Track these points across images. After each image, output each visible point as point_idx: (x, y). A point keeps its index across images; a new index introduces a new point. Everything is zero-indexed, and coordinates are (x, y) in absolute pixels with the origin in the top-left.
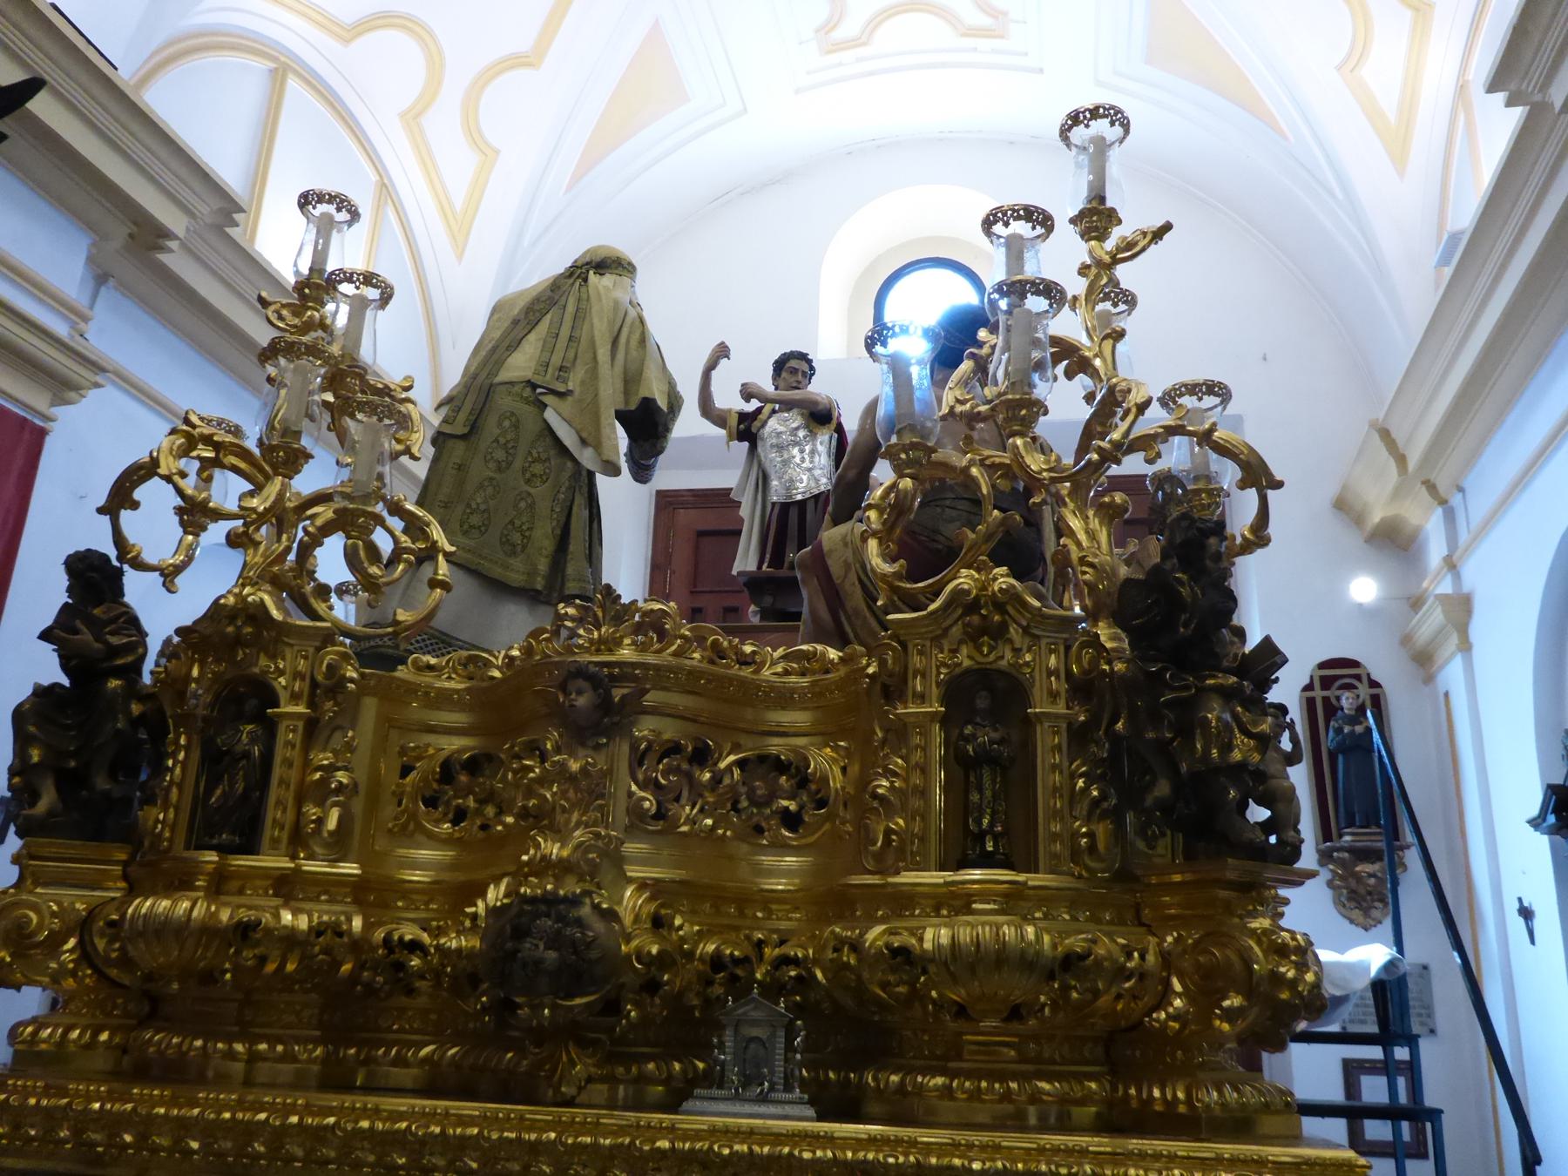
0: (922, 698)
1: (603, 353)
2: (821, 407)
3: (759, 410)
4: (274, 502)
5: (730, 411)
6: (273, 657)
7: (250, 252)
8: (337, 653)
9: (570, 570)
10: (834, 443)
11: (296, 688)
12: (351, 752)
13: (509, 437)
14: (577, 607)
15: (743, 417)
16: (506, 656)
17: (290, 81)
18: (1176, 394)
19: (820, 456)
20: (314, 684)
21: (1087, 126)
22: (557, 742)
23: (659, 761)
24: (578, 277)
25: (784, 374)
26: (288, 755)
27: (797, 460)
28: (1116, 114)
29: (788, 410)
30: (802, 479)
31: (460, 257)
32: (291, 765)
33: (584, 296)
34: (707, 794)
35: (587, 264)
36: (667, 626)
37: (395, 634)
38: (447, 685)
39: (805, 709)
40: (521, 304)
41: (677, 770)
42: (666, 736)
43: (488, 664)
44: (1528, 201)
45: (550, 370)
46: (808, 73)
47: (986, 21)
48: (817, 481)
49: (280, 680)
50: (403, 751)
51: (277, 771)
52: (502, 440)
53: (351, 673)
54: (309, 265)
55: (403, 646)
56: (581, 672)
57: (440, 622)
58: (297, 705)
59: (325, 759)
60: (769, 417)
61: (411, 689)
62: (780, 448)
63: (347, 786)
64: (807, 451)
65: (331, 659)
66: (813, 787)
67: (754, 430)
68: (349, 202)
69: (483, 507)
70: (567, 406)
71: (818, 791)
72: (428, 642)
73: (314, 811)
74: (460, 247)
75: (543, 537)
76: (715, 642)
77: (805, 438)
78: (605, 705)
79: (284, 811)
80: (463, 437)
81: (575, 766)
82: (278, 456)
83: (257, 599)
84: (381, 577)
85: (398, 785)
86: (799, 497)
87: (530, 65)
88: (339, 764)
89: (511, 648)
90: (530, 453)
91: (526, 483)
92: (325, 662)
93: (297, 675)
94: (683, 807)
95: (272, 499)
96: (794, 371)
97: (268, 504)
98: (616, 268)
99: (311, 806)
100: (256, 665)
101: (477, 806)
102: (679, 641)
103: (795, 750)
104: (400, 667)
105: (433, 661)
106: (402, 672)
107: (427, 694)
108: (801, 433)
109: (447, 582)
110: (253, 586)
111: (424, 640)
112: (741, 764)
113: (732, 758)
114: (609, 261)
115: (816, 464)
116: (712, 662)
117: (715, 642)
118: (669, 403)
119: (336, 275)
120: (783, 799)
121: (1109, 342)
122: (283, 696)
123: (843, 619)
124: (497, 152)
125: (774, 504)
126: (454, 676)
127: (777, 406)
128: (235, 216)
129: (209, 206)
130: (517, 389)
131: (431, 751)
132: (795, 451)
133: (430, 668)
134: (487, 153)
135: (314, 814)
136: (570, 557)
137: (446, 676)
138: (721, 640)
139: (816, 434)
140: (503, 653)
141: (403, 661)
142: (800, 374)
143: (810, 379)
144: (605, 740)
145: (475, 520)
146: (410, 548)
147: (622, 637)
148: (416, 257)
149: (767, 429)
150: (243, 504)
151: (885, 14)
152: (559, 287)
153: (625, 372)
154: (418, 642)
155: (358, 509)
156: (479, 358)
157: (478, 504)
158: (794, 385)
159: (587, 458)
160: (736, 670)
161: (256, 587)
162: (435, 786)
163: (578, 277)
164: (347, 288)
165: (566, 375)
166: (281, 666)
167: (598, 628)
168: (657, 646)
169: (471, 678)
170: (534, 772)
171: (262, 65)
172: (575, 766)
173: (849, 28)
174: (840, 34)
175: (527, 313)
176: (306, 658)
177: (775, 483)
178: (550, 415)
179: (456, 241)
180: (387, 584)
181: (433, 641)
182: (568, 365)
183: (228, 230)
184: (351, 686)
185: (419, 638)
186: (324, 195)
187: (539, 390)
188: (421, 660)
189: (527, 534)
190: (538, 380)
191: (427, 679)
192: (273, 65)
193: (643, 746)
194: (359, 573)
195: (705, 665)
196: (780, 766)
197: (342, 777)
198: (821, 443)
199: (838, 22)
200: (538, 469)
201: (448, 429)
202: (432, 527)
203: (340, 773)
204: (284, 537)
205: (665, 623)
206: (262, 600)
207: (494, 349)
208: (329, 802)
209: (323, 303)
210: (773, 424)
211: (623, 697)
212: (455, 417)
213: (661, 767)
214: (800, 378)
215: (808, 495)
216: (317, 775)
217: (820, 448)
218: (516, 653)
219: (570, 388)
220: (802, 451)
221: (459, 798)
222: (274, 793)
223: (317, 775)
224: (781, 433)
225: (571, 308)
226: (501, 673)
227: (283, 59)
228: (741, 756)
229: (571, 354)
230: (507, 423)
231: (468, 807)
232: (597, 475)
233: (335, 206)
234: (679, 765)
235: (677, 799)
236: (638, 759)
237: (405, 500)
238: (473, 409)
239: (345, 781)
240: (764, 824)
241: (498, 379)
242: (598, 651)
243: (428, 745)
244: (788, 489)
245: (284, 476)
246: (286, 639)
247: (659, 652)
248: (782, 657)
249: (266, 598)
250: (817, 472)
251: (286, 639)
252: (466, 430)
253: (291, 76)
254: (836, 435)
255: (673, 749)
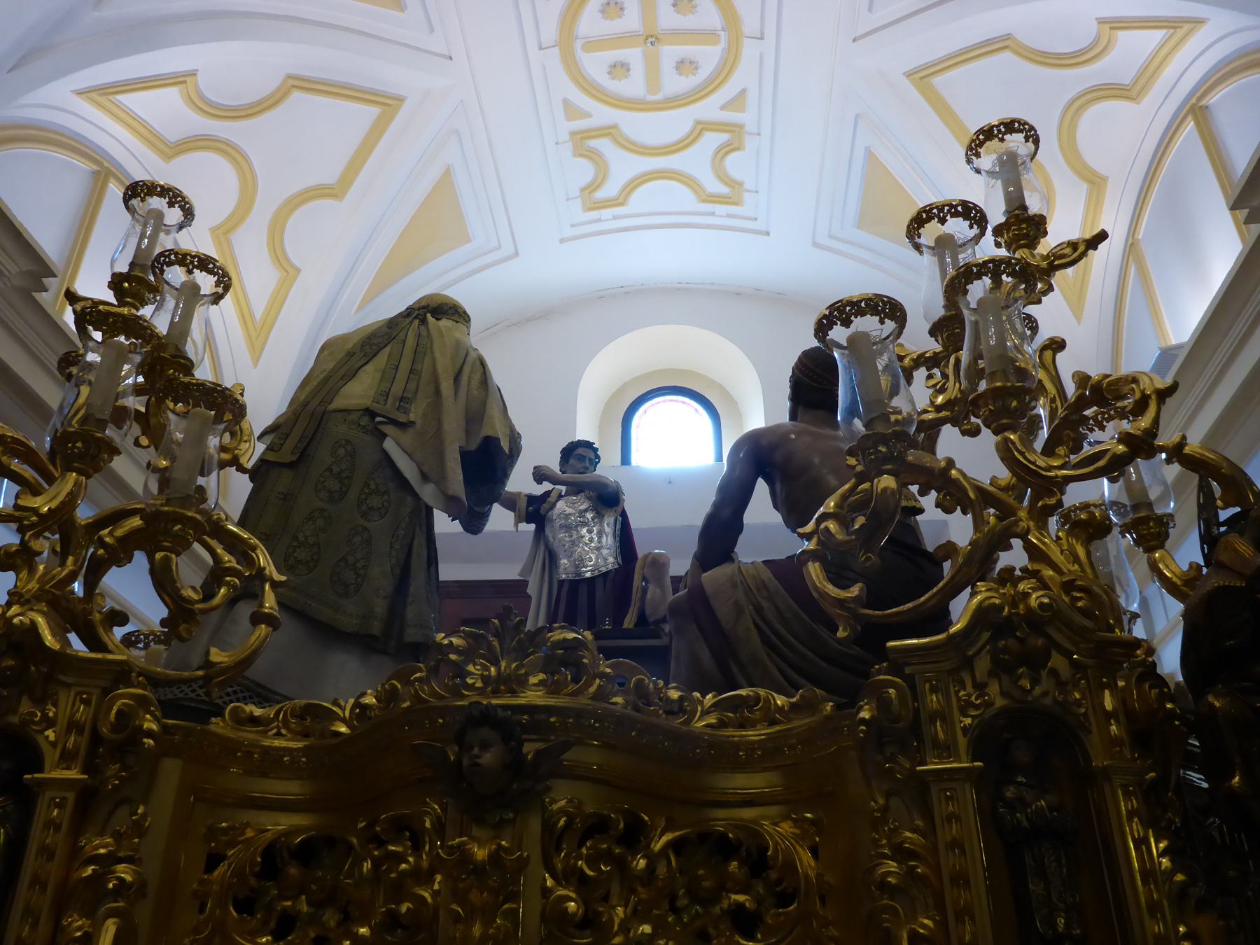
0: (946, 750)
1: (446, 386)
2: (610, 490)
3: (547, 494)
4: (62, 503)
5: (519, 494)
6: (40, 701)
7: (58, 322)
8: (131, 696)
9: (411, 613)
10: (618, 526)
11: (70, 744)
12: (139, 837)
13: (343, 466)
14: (467, 636)
15: (531, 499)
16: (357, 704)
17: (111, 184)
18: (1103, 418)
19: (607, 536)
20: (96, 739)
21: (1002, 140)
22: (439, 818)
23: (581, 845)
24: (416, 317)
25: (572, 461)
26: (48, 841)
27: (586, 539)
28: (1030, 130)
29: (576, 493)
30: (590, 558)
31: (256, 361)
32: (51, 856)
33: (424, 333)
34: (640, 889)
35: (424, 307)
36: (585, 661)
37: (207, 680)
38: (277, 743)
39: (765, 770)
40: (355, 339)
41: (607, 857)
42: (590, 809)
43: (333, 717)
44: (1247, 321)
45: (390, 400)
46: (572, 226)
47: (724, 190)
48: (605, 560)
49: (47, 733)
50: (212, 832)
51: (31, 862)
52: (336, 469)
53: (150, 725)
54: (131, 260)
55: (216, 692)
56: (485, 717)
57: (256, 672)
58: (68, 768)
59: (102, 846)
60: (557, 501)
61: (229, 748)
62: (568, 528)
63: (132, 884)
64: (595, 532)
65: (124, 704)
66: (774, 875)
67: (542, 511)
68: (184, 198)
69: (311, 540)
70: (407, 437)
71: (780, 881)
72: (240, 695)
73: (80, 923)
74: (256, 351)
75: (380, 576)
76: (640, 683)
77: (593, 519)
78: (515, 765)
79: (35, 926)
80: (291, 465)
81: (480, 853)
82: (74, 447)
83: (27, 621)
84: (197, 602)
85: (202, 882)
86: (588, 575)
87: (334, 196)
88: (121, 854)
89: (364, 694)
90: (367, 485)
91: (362, 517)
92: (115, 709)
93: (74, 726)
94: (614, 907)
95: (61, 498)
96: (582, 458)
97: (54, 505)
98: (453, 315)
99: (76, 917)
100: (15, 712)
101: (312, 910)
102: (598, 681)
103: (743, 826)
104: (213, 720)
105: (258, 712)
106: (217, 726)
107: (249, 754)
108: (589, 515)
109: (275, 617)
110: (22, 605)
111: (235, 692)
112: (675, 845)
113: (665, 839)
114: (445, 307)
115: (604, 544)
116: (637, 709)
117: (640, 683)
118: (510, 446)
119: (165, 257)
120: (736, 893)
121: (1048, 353)
122: (51, 756)
123: (735, 669)
124: (298, 270)
125: (562, 582)
126: (284, 732)
127: (563, 488)
128: (44, 280)
129: (17, 265)
130: (354, 416)
131: (250, 833)
132: (584, 530)
133: (254, 720)
134: (288, 271)
135: (79, 929)
136: (410, 600)
137: (274, 731)
138: (647, 681)
139: (604, 516)
140: (352, 701)
141: (219, 713)
142: (587, 461)
143: (596, 466)
144: (511, 815)
145: (302, 554)
146: (235, 569)
147: (527, 675)
148: (214, 351)
149: (556, 511)
150: (19, 502)
151: (642, 179)
152: (397, 324)
153: (467, 409)
154: (228, 694)
155: (174, 513)
156: (308, 389)
157: (306, 537)
158: (581, 471)
159: (427, 493)
160: (663, 720)
161: (26, 607)
162: (253, 882)
163: (416, 317)
164: (175, 275)
165: (407, 406)
166: (51, 714)
167: (496, 663)
168: (572, 687)
169: (306, 735)
170: (407, 862)
171: (85, 166)
172: (480, 853)
173: (609, 190)
174: (601, 194)
175: (362, 346)
176: (87, 703)
177: (564, 561)
178: (389, 445)
179: (253, 348)
180: (204, 612)
181: (247, 694)
182: (410, 396)
183: (35, 294)
184: (150, 742)
185: (230, 690)
186: (156, 187)
187: (378, 419)
188: (244, 711)
189: (362, 572)
190: (377, 407)
191: (250, 736)
192: (95, 168)
193: (562, 822)
194: (169, 595)
195: (629, 711)
196: (724, 847)
197: (124, 872)
198: (608, 525)
199: (601, 183)
200: (375, 501)
201: (271, 457)
202: (258, 551)
203: (121, 867)
204: (70, 559)
205: (584, 657)
206: (33, 624)
207: (327, 379)
208: (103, 910)
209: (144, 300)
210: (561, 505)
211: (538, 753)
212: (282, 445)
213: (584, 851)
214: (587, 464)
215: (596, 573)
216: (89, 870)
217: (607, 529)
218: (370, 700)
219: (412, 419)
220: (590, 532)
221: (287, 900)
222: (23, 894)
223: (89, 870)
224: (570, 514)
225: (411, 341)
226: (348, 726)
227: (106, 164)
228: (677, 834)
229: (412, 386)
230: (342, 451)
231: (299, 911)
232: (435, 511)
233: (167, 200)
234: (609, 849)
235: (606, 899)
236: (552, 840)
237: (227, 520)
238: (302, 437)
239: (128, 878)
240: (711, 931)
241: (332, 406)
242: (496, 693)
243: (248, 825)
244: (577, 567)
245: (80, 472)
246: (62, 677)
247: (572, 694)
248: (714, 705)
249: (40, 620)
250: (605, 552)
251: (62, 677)
252: (294, 458)
253: (112, 180)
254: (620, 519)
255: (598, 826)
